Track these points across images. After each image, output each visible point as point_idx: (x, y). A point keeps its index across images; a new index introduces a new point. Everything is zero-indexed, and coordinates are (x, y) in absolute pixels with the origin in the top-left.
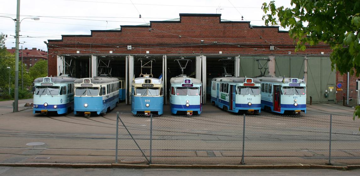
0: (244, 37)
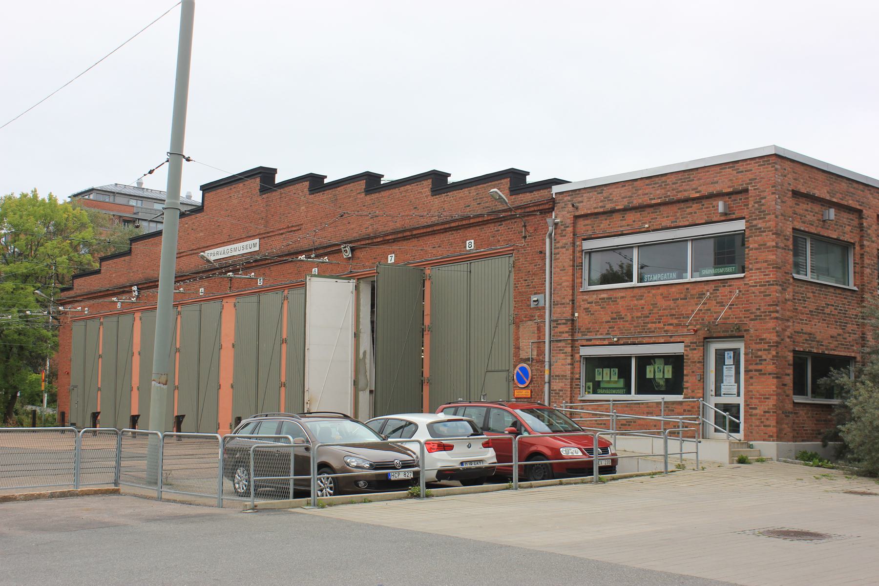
0: (298, 228)
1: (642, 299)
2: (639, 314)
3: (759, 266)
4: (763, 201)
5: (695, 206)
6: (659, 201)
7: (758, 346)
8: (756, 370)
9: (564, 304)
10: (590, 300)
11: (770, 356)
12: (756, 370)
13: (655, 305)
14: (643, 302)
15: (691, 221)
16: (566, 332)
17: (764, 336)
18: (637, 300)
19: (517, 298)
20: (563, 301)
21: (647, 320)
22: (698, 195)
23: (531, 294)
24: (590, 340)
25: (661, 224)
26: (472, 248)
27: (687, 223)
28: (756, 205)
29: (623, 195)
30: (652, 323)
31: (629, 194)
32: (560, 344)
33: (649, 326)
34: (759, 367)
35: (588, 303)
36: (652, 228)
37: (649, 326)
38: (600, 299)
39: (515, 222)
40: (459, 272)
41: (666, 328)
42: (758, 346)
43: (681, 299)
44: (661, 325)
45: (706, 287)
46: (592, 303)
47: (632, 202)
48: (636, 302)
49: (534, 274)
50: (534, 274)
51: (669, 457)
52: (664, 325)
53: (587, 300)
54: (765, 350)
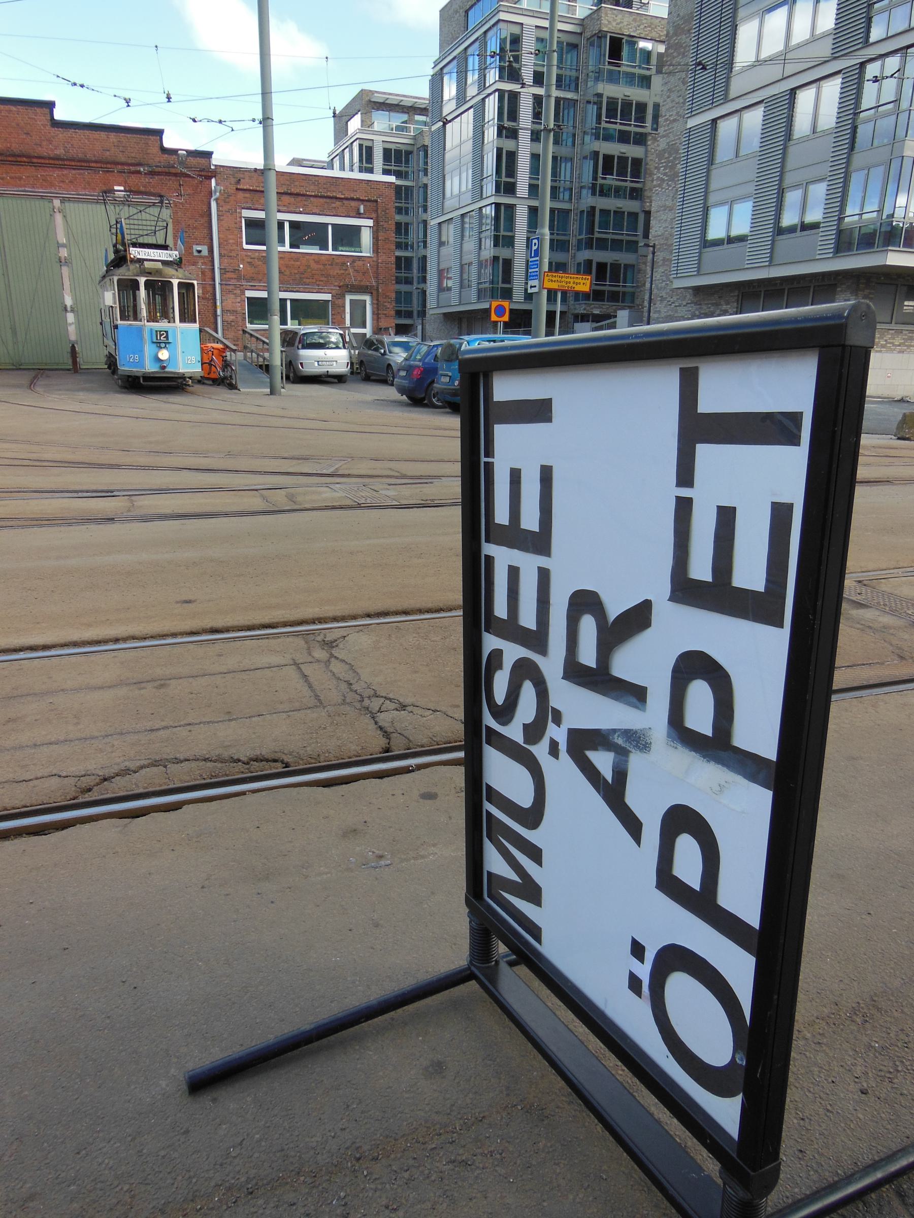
1: (298, 261)
2: (296, 271)
3: (385, 251)
4: (387, 211)
5: (338, 203)
6: (313, 194)
7: (385, 300)
8: (383, 314)
9: (231, 256)
10: (253, 256)
11: (392, 306)
12: (383, 314)
13: (308, 266)
14: (298, 263)
15: (335, 213)
16: (235, 278)
17: (388, 294)
18: (294, 261)
19: (564, 300)
20: (231, 254)
21: (303, 276)
22: (343, 197)
23: (193, 244)
24: (255, 286)
25: (312, 210)
26: (590, 277)
27: (332, 214)
28: (383, 213)
29: (282, 182)
30: (307, 278)
31: (288, 183)
32: (228, 287)
33: (304, 280)
34: (385, 312)
35: (251, 258)
36: (305, 212)
37: (304, 280)
38: (262, 257)
39: (170, 179)
40: (143, 218)
41: (318, 283)
42: (385, 300)
43: (329, 265)
44: (314, 281)
45: (347, 260)
46: (254, 258)
47: (290, 190)
48: (293, 263)
49: (195, 228)
50: (195, 228)
51: (70, 365)
52: (317, 281)
53: (250, 256)
54: (389, 302)
